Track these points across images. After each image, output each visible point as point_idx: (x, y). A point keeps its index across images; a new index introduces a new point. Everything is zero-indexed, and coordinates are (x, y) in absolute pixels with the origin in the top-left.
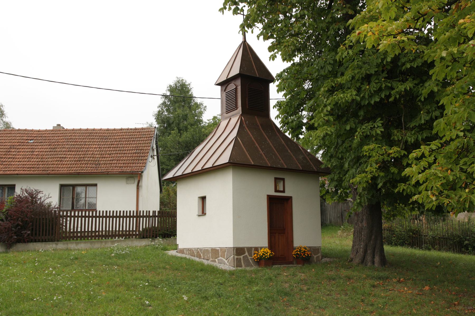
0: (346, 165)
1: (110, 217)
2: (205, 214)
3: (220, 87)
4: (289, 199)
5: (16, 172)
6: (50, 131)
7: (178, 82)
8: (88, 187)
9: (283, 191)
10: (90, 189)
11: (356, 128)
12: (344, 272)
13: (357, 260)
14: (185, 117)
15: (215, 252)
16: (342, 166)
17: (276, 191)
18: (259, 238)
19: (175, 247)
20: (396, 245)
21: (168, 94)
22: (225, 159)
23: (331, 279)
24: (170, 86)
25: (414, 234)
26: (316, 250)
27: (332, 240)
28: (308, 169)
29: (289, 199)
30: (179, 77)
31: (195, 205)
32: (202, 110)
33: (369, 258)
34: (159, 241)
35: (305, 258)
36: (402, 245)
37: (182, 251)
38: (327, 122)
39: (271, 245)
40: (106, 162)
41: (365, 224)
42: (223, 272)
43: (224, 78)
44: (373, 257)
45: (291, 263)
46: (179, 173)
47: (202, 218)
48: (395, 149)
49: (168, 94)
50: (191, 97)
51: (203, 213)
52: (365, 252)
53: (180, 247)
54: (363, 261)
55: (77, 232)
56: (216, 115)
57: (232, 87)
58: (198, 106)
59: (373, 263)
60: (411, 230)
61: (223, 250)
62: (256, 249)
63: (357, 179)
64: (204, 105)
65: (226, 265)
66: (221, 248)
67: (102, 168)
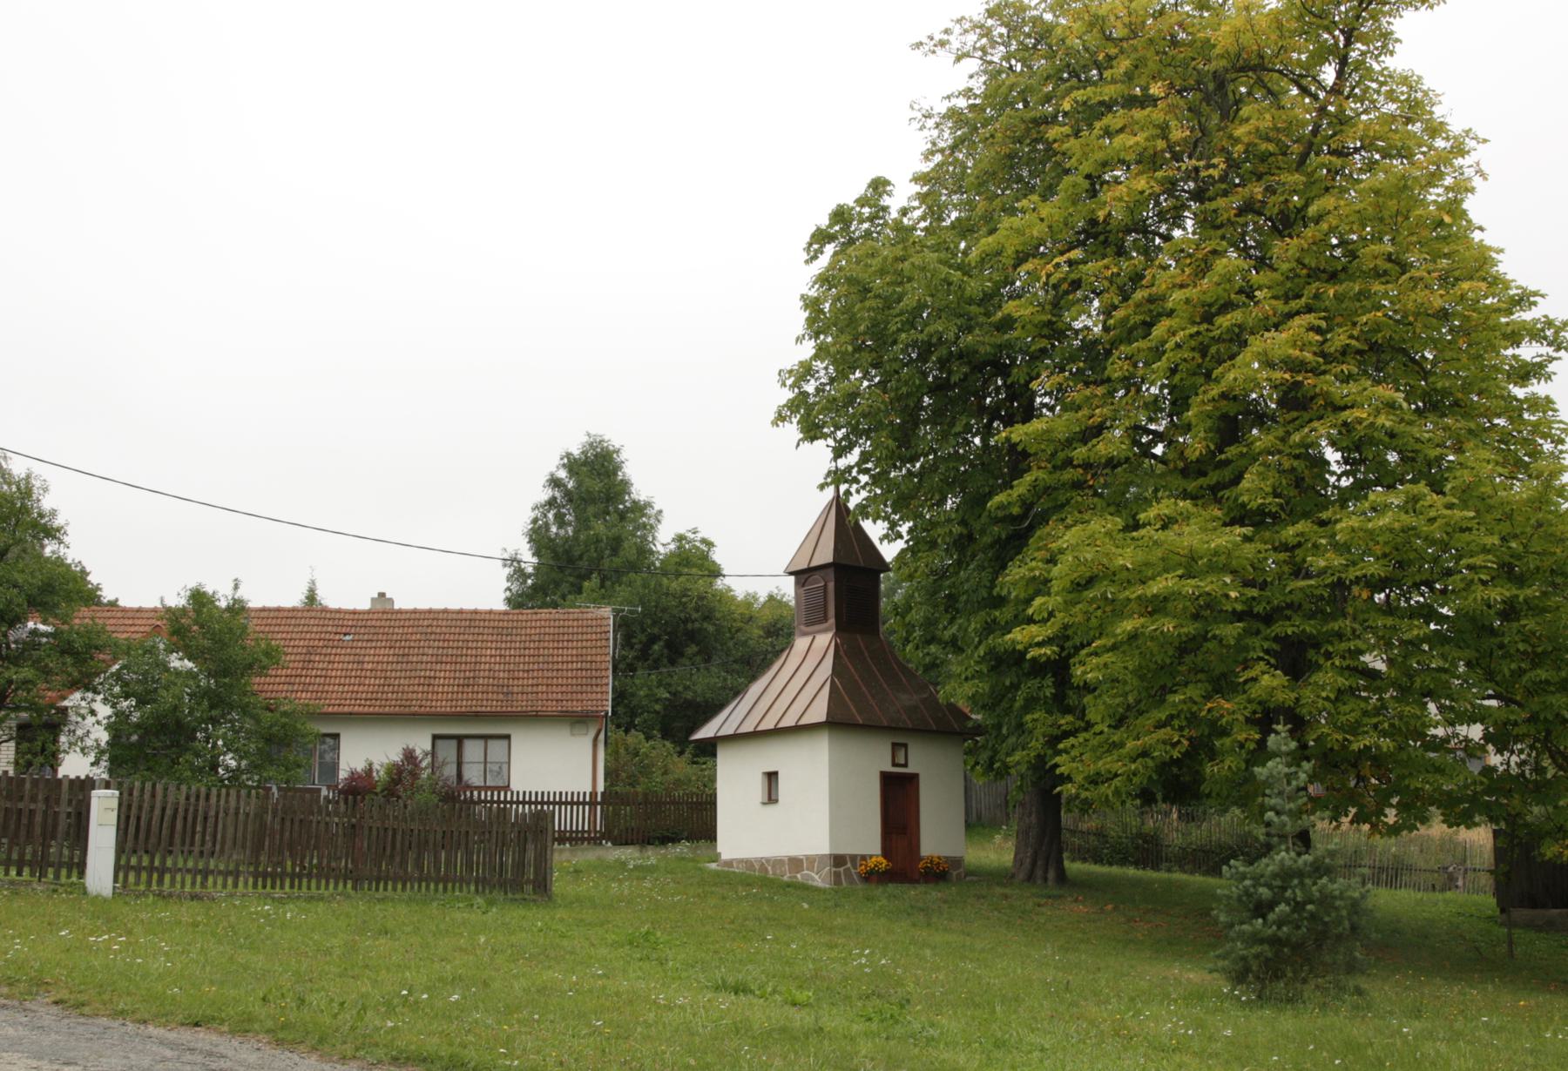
0: (1004, 731)
1: (566, 803)
2: (776, 801)
3: (792, 578)
4: (913, 779)
5: (346, 709)
6: (364, 612)
7: (591, 444)
8: (490, 742)
9: (905, 765)
10: (496, 748)
11: (1020, 683)
12: (998, 890)
13: (1021, 876)
14: (616, 544)
15: (796, 863)
16: (999, 726)
17: (894, 765)
18: (868, 842)
19: (716, 858)
20: (1111, 864)
21: (562, 474)
22: (823, 719)
23: (979, 897)
24: (568, 455)
25: (1145, 841)
26: (957, 862)
27: (982, 854)
28: (945, 726)
29: (913, 779)
30: (593, 432)
31: (758, 787)
32: (652, 521)
33: (1039, 872)
34: (682, 849)
35: (938, 873)
36: (1123, 862)
37: (729, 863)
38: (978, 675)
39: (886, 852)
40: (526, 689)
41: (1033, 818)
42: (817, 889)
43: (803, 565)
44: (1046, 871)
45: (917, 882)
46: (728, 730)
47: (771, 808)
48: (1070, 718)
49: (562, 474)
50: (625, 485)
51: (771, 798)
52: (1034, 863)
53: (725, 856)
54: (1030, 878)
55: (583, 831)
56: (682, 531)
57: (817, 582)
58: (640, 508)
59: (1046, 879)
60: (1140, 835)
61: (811, 859)
62: (864, 858)
63: (1017, 756)
64: (657, 507)
65: (819, 879)
66: (807, 857)
67: (521, 705)
